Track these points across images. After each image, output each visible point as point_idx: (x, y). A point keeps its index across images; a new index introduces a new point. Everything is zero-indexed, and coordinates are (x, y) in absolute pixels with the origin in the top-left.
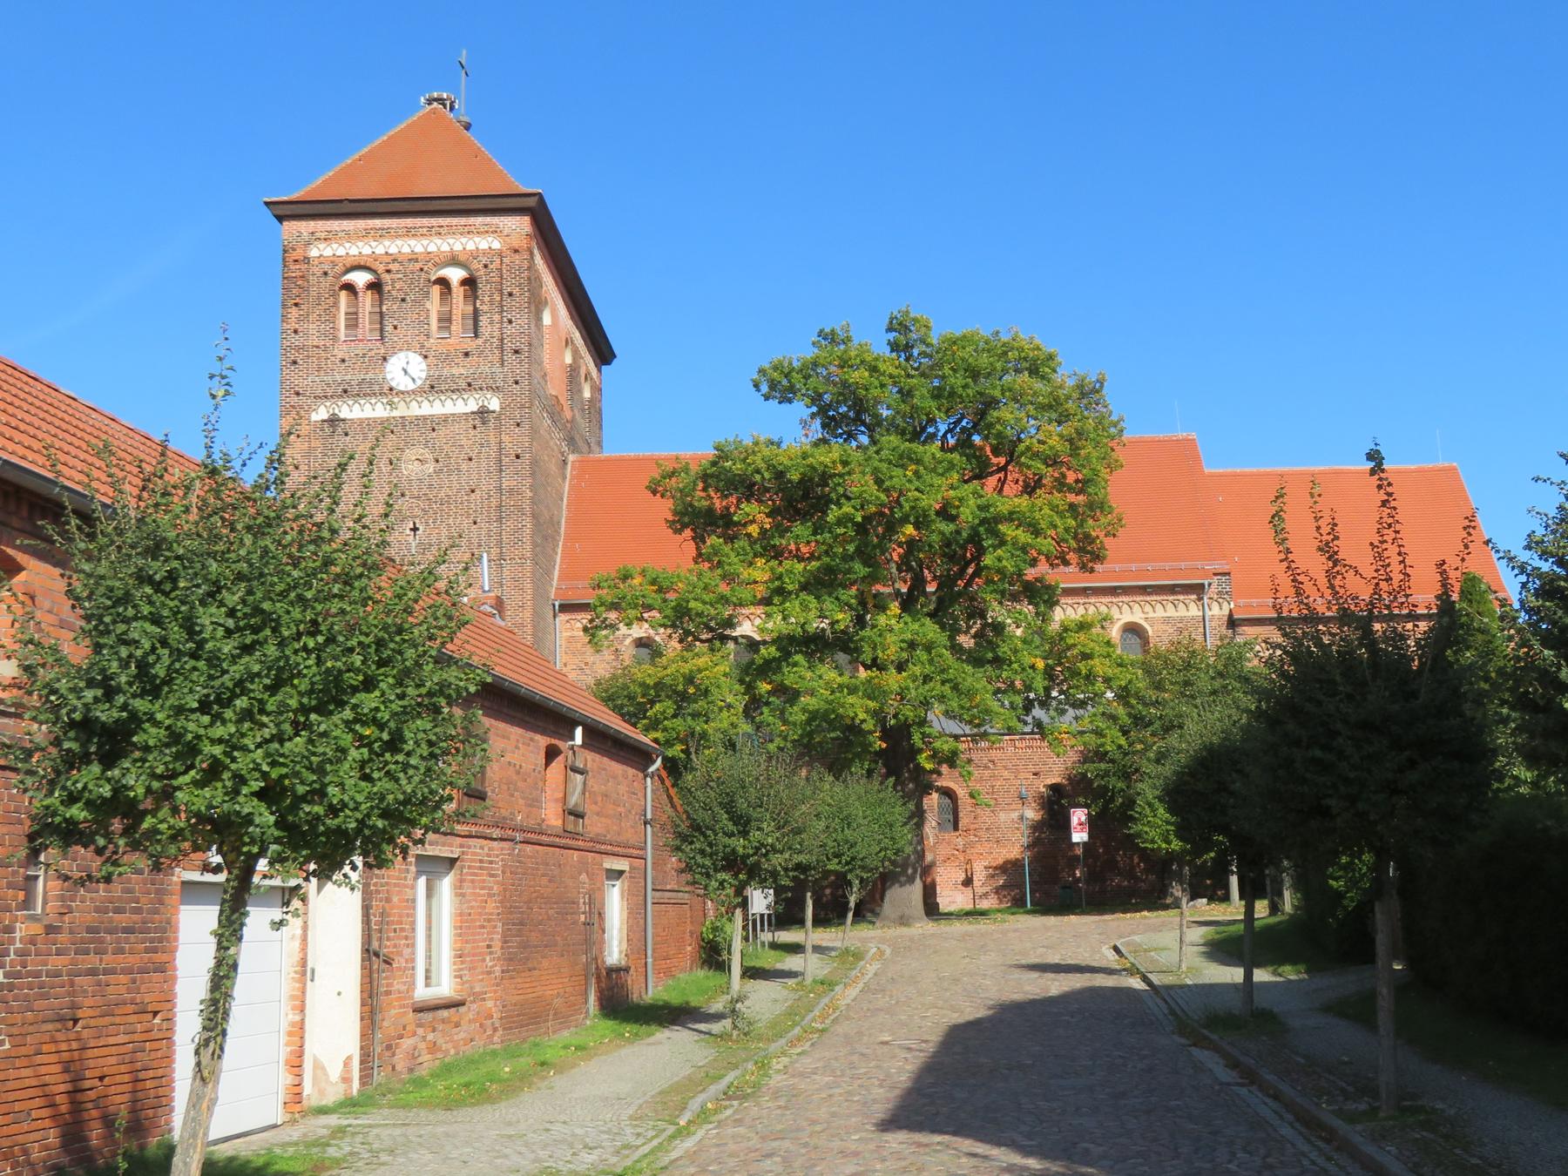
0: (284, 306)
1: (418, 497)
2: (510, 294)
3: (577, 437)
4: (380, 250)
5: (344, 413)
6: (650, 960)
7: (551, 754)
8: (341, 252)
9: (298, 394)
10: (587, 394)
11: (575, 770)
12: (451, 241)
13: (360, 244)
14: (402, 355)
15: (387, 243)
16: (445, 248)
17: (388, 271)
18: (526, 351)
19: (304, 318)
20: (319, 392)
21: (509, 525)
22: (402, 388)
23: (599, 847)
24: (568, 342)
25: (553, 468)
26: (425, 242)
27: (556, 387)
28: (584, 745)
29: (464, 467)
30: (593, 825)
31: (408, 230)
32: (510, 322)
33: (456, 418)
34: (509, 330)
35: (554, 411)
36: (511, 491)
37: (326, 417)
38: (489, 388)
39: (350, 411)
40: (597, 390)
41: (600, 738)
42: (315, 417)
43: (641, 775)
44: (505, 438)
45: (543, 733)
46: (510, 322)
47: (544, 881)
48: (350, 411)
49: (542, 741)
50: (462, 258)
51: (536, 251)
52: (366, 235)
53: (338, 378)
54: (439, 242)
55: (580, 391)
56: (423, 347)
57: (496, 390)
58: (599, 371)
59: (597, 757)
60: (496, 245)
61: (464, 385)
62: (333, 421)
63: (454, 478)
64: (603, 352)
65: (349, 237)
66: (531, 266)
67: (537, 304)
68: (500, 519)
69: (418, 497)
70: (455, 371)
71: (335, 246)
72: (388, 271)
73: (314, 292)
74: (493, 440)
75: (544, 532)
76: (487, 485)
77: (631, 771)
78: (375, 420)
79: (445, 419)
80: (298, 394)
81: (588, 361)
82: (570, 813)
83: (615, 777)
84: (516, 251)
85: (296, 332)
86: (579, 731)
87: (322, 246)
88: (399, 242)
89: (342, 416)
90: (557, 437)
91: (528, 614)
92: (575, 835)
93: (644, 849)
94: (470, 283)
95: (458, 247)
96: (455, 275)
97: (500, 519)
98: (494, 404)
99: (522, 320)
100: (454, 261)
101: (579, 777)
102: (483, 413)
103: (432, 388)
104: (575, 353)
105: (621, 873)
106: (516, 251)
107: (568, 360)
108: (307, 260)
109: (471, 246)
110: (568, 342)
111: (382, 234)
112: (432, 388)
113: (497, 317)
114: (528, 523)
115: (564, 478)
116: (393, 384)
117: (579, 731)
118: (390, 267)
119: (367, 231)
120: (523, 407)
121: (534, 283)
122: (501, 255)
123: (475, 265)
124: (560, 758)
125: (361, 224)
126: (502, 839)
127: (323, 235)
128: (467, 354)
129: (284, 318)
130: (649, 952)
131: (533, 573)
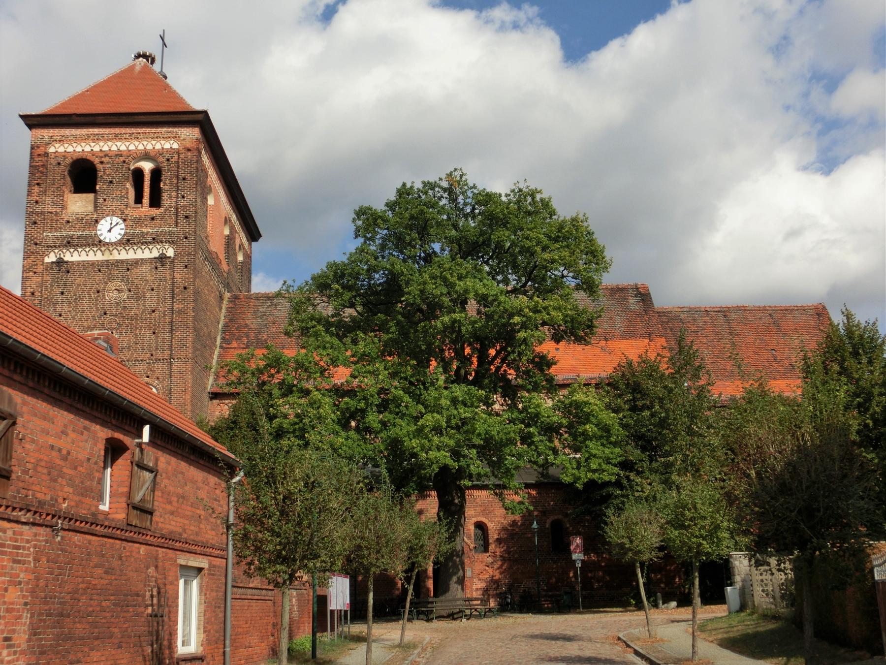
0: (30, 185)
1: (116, 315)
2: (184, 179)
3: (232, 285)
4: (97, 149)
5: (67, 257)
6: (228, 649)
7: (114, 450)
8: (70, 149)
9: (36, 244)
10: (240, 258)
11: (142, 467)
12: (145, 143)
13: (83, 144)
14: (108, 218)
15: (101, 144)
16: (141, 147)
17: (102, 163)
18: (194, 217)
19: (44, 193)
20: (50, 242)
21: (177, 334)
22: (107, 240)
23: (173, 542)
24: (227, 221)
25: (213, 300)
26: (127, 144)
27: (217, 246)
28: (152, 442)
29: (148, 295)
30: (165, 521)
31: (116, 135)
32: (183, 197)
33: (143, 261)
34: (182, 203)
35: (212, 259)
36: (180, 312)
37: (54, 259)
38: (167, 241)
39: (72, 256)
40: (248, 257)
41: (169, 438)
42: (47, 260)
43: (224, 485)
44: (177, 275)
45: (104, 424)
46: (183, 197)
47: (99, 571)
48: (72, 256)
49: (102, 433)
50: (152, 154)
51: (203, 152)
52: (87, 138)
53: (64, 234)
54: (137, 143)
55: (235, 255)
56: (123, 213)
57: (172, 243)
58: (250, 244)
59: (173, 460)
60: (175, 146)
61: (150, 239)
62: (60, 262)
63: (141, 302)
64: (253, 234)
65: (76, 139)
66: (199, 160)
67: (205, 190)
68: (171, 331)
69: (116, 315)
70: (145, 230)
71: (66, 145)
72: (102, 163)
73: (51, 175)
74: (169, 277)
75: (203, 344)
76: (163, 307)
77: (213, 480)
78: (88, 262)
79: (137, 262)
80: (36, 244)
81: (241, 237)
82: (135, 508)
83: (194, 482)
84: (189, 150)
85: (37, 202)
86: (146, 429)
87: (57, 145)
88: (110, 143)
89: (66, 259)
90: (215, 282)
91: (188, 397)
92: (141, 531)
93: (227, 550)
94: (156, 174)
95: (149, 147)
96: (147, 167)
97: (171, 331)
98: (170, 253)
99: (190, 196)
100: (146, 156)
101: (147, 475)
102: (162, 258)
103: (127, 241)
104: (232, 228)
105: (200, 570)
106: (189, 150)
107: (227, 232)
108: (46, 154)
109: (158, 147)
110: (227, 221)
111: (98, 138)
112: (127, 241)
113: (174, 194)
114: (191, 336)
115: (221, 309)
116: (102, 238)
117: (146, 429)
118: (103, 159)
119: (88, 136)
120: (190, 254)
121: (201, 172)
122: (178, 152)
123: (161, 159)
124: (127, 455)
125: (84, 131)
126: (34, 524)
127: (58, 138)
128: (153, 219)
129: (29, 193)
130: (228, 642)
131: (193, 369)
